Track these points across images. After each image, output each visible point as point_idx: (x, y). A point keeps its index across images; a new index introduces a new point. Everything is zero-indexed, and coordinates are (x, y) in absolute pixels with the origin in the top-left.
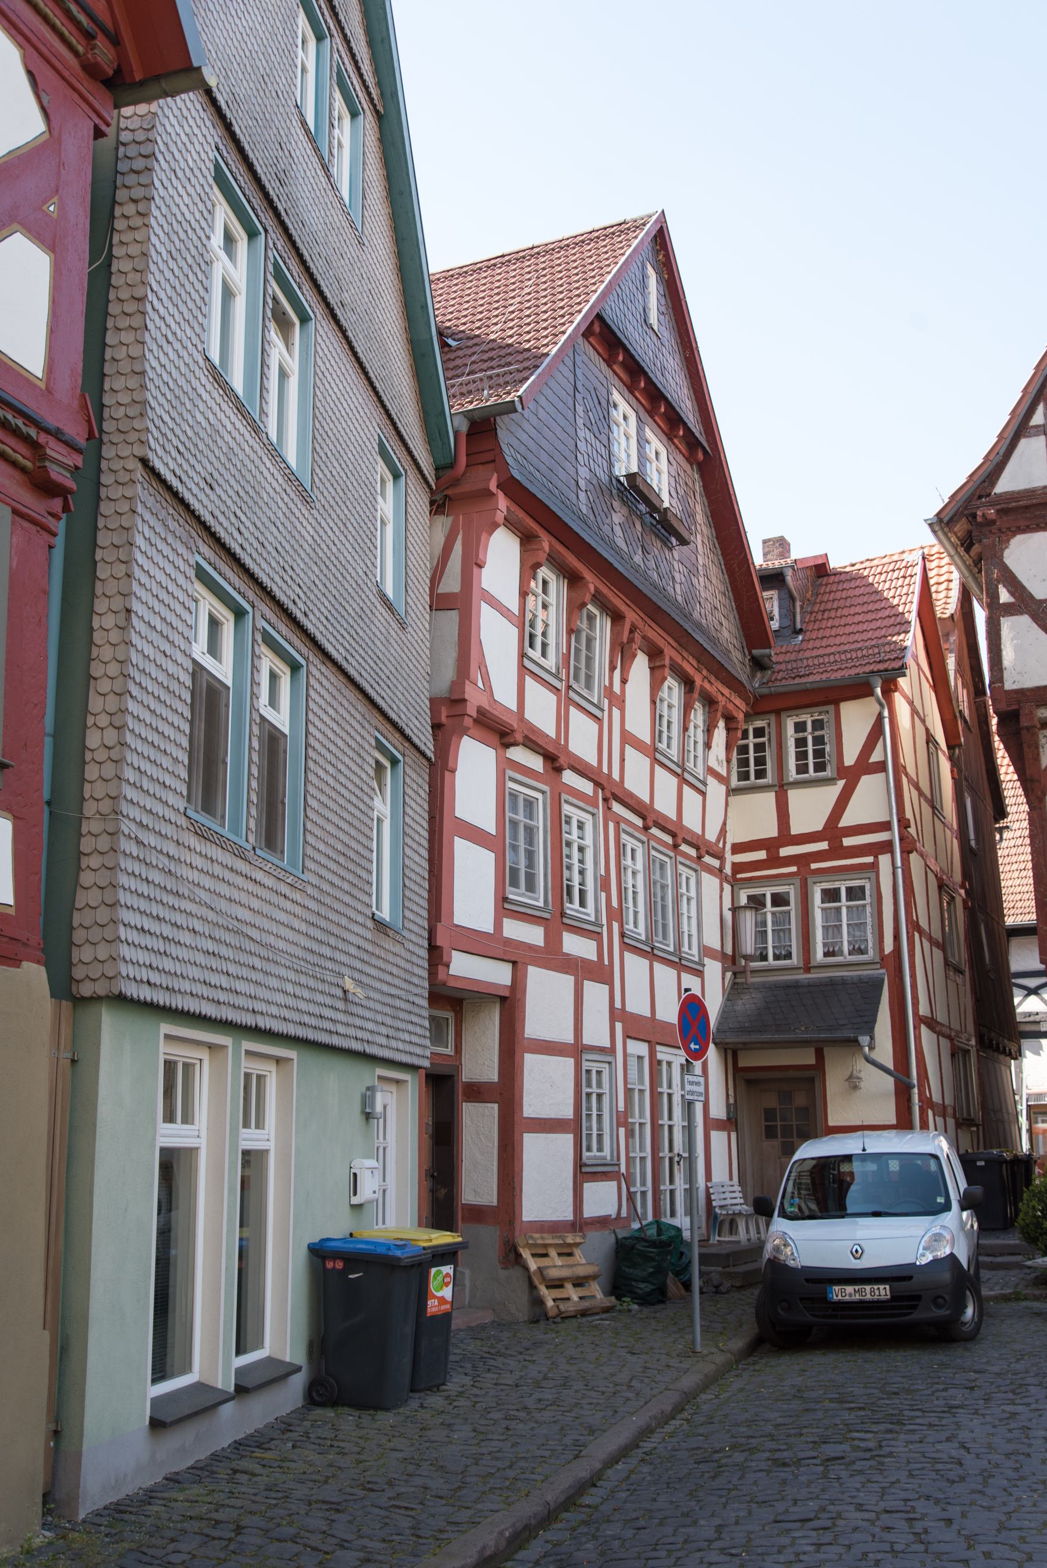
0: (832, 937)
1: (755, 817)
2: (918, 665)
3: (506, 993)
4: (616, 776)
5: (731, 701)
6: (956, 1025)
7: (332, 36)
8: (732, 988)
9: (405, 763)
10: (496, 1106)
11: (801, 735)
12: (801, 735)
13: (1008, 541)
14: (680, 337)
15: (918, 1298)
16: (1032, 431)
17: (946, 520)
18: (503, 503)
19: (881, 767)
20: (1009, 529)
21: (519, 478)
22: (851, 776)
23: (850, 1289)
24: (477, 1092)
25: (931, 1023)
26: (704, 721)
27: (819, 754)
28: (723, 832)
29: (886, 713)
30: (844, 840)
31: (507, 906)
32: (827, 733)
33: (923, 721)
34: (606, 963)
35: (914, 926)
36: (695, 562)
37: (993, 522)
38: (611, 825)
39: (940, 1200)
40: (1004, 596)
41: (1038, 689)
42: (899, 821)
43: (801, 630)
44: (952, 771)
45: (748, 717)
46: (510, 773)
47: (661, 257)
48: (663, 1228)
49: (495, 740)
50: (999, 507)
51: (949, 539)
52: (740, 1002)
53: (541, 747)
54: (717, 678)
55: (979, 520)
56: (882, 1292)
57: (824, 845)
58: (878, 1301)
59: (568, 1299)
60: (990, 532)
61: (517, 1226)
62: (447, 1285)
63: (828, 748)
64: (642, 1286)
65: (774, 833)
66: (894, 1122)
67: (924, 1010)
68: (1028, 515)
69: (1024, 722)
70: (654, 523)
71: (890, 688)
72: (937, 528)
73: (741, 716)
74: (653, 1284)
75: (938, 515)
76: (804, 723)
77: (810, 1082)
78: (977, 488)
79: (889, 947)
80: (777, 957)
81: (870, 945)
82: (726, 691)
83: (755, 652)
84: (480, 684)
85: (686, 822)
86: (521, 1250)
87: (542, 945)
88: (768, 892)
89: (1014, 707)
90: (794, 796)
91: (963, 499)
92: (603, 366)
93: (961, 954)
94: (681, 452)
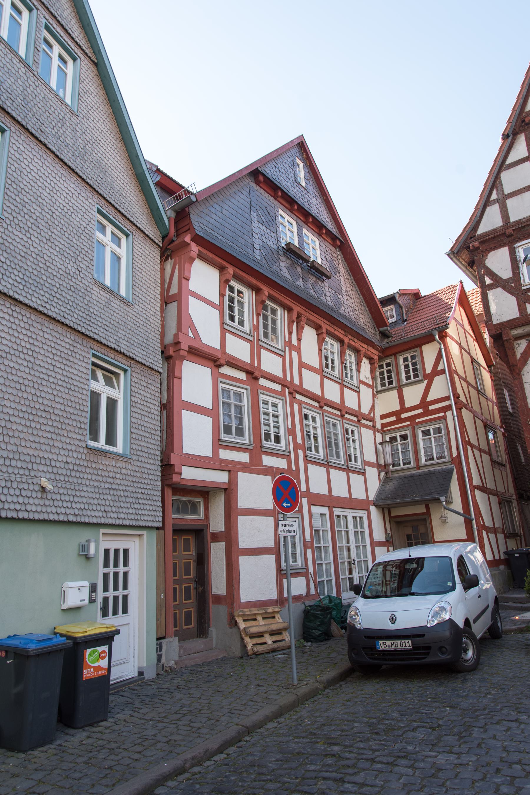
0: (426, 450)
1: (389, 402)
2: (465, 330)
3: (226, 487)
4: (296, 381)
5: (368, 350)
6: (501, 489)
7: (37, 9)
8: (385, 480)
9: (131, 371)
10: (224, 543)
11: (406, 363)
12: (406, 363)
13: (487, 255)
14: (321, 191)
15: (429, 648)
16: (492, 203)
17: (455, 252)
18: (195, 248)
19: (443, 372)
20: (486, 250)
21: (202, 235)
22: (430, 378)
23: (388, 643)
24: (216, 537)
25: (483, 489)
26: (355, 360)
27: (415, 370)
28: (373, 409)
29: (442, 347)
30: (430, 407)
31: (221, 443)
32: (418, 360)
33: (469, 353)
34: (294, 469)
35: (467, 443)
36: (340, 289)
37: (478, 248)
38: (296, 406)
39: (450, 584)
40: (488, 281)
41: (509, 321)
42: (454, 395)
43: (406, 320)
44: (491, 377)
45: (381, 359)
46: (220, 379)
47: (304, 156)
48: (332, 599)
49: (211, 364)
50: (480, 241)
51: (461, 263)
52: (388, 486)
53: (244, 368)
54: (358, 340)
55: (470, 250)
56: (407, 644)
57: (421, 411)
58: (405, 650)
59: (265, 643)
60: (478, 253)
61: (236, 605)
62: (103, 658)
63: (418, 367)
64: (314, 631)
65: (398, 408)
66: (466, 537)
67: (476, 481)
68: (495, 241)
69: (505, 338)
70: (309, 268)
71: (443, 336)
72: (452, 256)
73: (376, 358)
74: (320, 631)
75: (451, 250)
76: (407, 358)
77: (424, 520)
78: (469, 234)
79: (455, 454)
80: (404, 464)
81: (446, 454)
82: (366, 346)
83: (381, 329)
84: (191, 334)
85: (347, 404)
86: (237, 619)
87: (286, 468)
88: (398, 435)
89: (499, 332)
90: (405, 390)
91: (463, 240)
92: (272, 199)
93: (503, 456)
94: (328, 242)
